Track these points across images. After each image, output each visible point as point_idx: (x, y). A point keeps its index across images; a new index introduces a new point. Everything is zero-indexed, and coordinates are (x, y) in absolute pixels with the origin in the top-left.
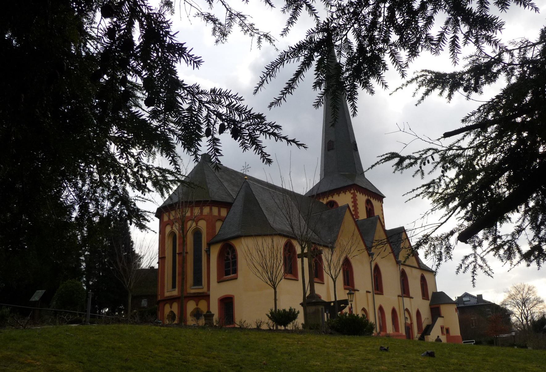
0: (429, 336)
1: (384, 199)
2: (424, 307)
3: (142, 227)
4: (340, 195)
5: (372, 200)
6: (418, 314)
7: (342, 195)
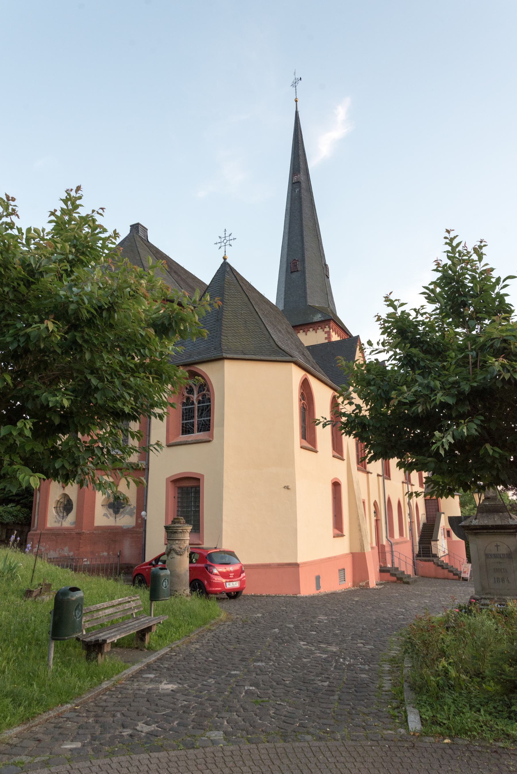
4: (308, 333)
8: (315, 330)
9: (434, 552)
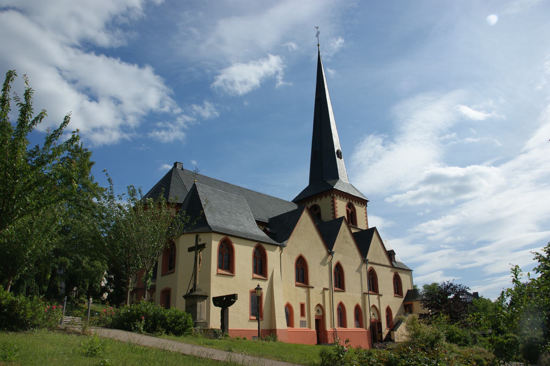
0: (395, 332)
1: (368, 203)
2: (396, 304)
3: (441, 275)
4: (322, 199)
5: (354, 203)
6: (388, 310)
7: (324, 199)
8: (326, 197)
9: (392, 338)
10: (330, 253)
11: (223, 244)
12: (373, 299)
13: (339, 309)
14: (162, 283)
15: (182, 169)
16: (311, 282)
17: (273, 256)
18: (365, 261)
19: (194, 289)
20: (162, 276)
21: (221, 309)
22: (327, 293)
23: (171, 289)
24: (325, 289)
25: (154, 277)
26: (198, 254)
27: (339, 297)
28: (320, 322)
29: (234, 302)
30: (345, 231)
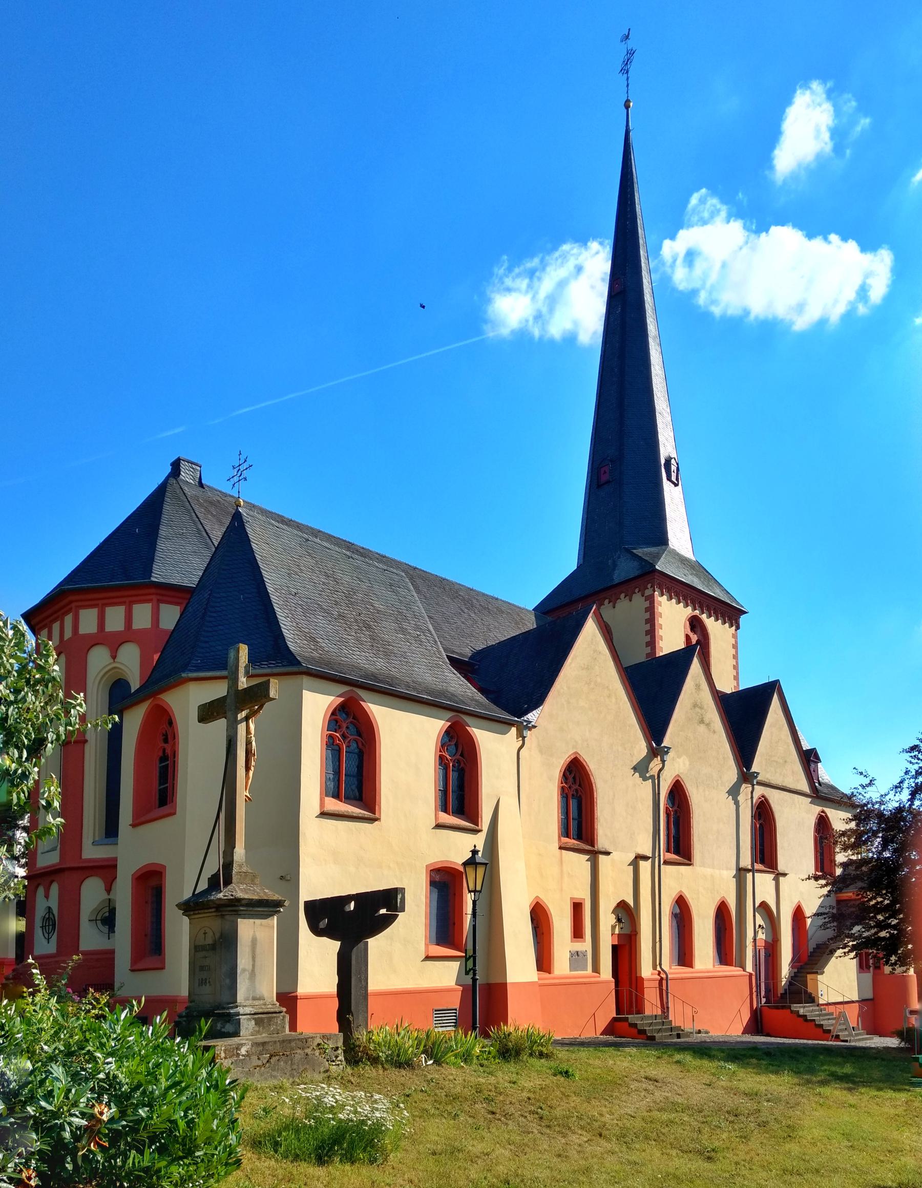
1: (743, 618)
5: (704, 617)
6: (798, 914)
7: (623, 604)
10: (657, 749)
11: (341, 717)
12: (763, 886)
13: (674, 915)
14: (134, 849)
15: (201, 485)
16: (603, 840)
17: (494, 747)
18: (746, 776)
19: (225, 876)
20: (134, 825)
21: (337, 945)
22: (645, 867)
23: (164, 867)
24: (640, 857)
25: (111, 829)
26: (242, 728)
27: (676, 880)
28: (625, 952)
29: (388, 921)
30: (698, 687)
